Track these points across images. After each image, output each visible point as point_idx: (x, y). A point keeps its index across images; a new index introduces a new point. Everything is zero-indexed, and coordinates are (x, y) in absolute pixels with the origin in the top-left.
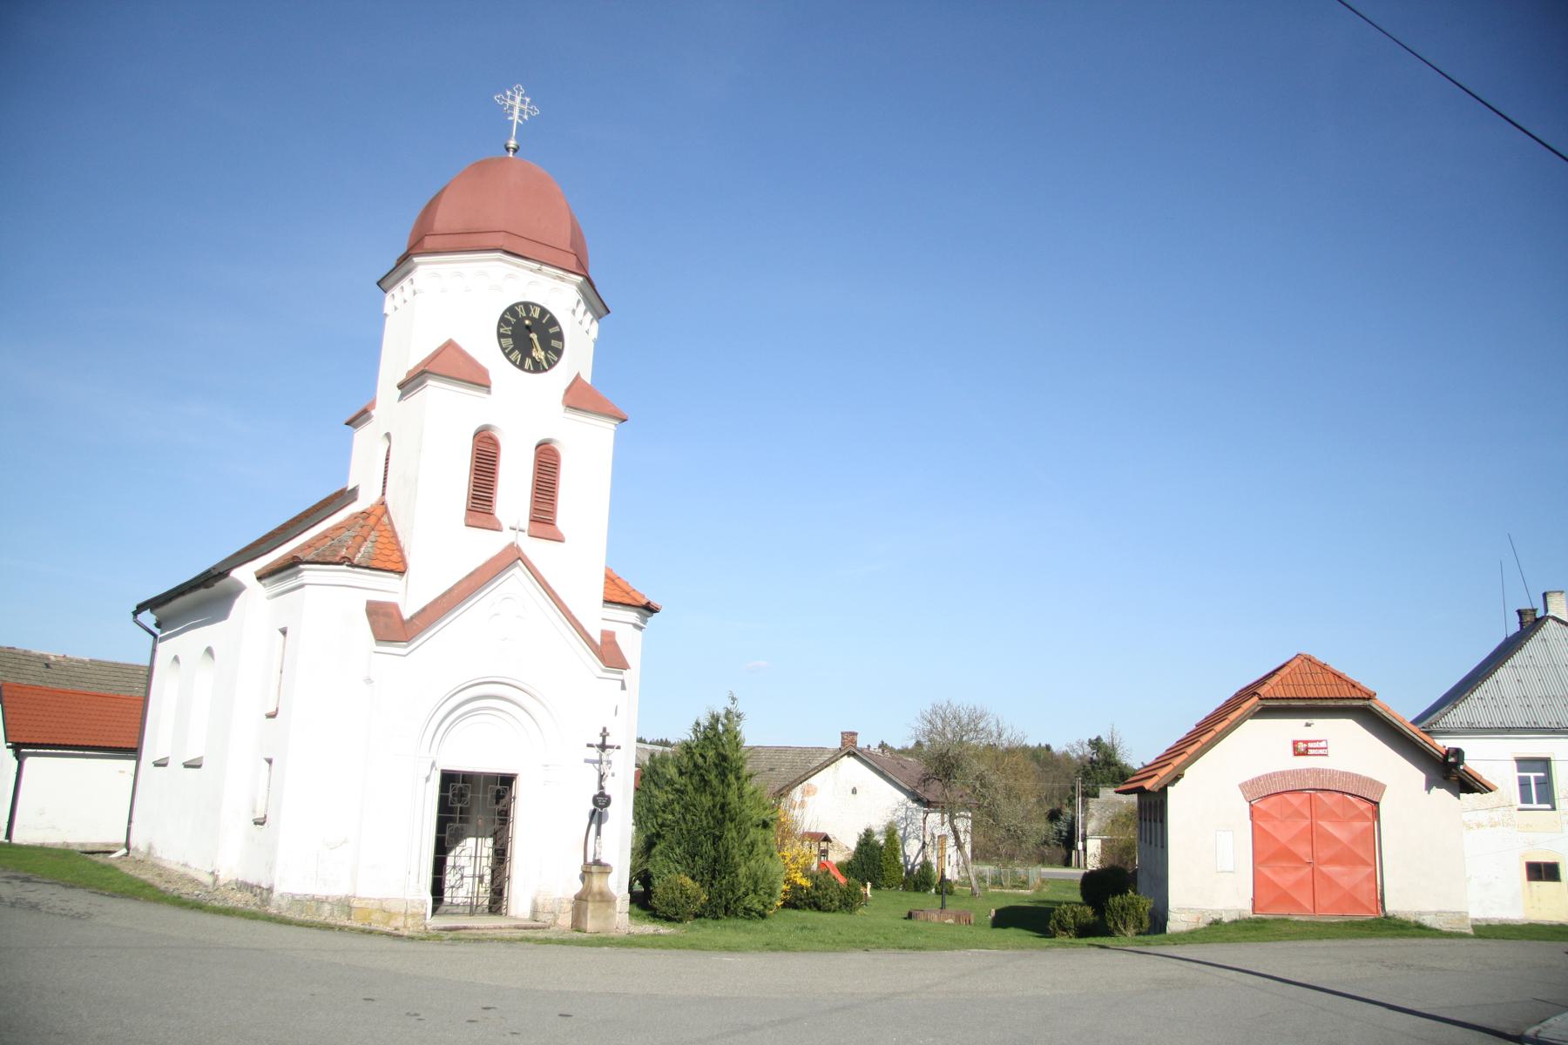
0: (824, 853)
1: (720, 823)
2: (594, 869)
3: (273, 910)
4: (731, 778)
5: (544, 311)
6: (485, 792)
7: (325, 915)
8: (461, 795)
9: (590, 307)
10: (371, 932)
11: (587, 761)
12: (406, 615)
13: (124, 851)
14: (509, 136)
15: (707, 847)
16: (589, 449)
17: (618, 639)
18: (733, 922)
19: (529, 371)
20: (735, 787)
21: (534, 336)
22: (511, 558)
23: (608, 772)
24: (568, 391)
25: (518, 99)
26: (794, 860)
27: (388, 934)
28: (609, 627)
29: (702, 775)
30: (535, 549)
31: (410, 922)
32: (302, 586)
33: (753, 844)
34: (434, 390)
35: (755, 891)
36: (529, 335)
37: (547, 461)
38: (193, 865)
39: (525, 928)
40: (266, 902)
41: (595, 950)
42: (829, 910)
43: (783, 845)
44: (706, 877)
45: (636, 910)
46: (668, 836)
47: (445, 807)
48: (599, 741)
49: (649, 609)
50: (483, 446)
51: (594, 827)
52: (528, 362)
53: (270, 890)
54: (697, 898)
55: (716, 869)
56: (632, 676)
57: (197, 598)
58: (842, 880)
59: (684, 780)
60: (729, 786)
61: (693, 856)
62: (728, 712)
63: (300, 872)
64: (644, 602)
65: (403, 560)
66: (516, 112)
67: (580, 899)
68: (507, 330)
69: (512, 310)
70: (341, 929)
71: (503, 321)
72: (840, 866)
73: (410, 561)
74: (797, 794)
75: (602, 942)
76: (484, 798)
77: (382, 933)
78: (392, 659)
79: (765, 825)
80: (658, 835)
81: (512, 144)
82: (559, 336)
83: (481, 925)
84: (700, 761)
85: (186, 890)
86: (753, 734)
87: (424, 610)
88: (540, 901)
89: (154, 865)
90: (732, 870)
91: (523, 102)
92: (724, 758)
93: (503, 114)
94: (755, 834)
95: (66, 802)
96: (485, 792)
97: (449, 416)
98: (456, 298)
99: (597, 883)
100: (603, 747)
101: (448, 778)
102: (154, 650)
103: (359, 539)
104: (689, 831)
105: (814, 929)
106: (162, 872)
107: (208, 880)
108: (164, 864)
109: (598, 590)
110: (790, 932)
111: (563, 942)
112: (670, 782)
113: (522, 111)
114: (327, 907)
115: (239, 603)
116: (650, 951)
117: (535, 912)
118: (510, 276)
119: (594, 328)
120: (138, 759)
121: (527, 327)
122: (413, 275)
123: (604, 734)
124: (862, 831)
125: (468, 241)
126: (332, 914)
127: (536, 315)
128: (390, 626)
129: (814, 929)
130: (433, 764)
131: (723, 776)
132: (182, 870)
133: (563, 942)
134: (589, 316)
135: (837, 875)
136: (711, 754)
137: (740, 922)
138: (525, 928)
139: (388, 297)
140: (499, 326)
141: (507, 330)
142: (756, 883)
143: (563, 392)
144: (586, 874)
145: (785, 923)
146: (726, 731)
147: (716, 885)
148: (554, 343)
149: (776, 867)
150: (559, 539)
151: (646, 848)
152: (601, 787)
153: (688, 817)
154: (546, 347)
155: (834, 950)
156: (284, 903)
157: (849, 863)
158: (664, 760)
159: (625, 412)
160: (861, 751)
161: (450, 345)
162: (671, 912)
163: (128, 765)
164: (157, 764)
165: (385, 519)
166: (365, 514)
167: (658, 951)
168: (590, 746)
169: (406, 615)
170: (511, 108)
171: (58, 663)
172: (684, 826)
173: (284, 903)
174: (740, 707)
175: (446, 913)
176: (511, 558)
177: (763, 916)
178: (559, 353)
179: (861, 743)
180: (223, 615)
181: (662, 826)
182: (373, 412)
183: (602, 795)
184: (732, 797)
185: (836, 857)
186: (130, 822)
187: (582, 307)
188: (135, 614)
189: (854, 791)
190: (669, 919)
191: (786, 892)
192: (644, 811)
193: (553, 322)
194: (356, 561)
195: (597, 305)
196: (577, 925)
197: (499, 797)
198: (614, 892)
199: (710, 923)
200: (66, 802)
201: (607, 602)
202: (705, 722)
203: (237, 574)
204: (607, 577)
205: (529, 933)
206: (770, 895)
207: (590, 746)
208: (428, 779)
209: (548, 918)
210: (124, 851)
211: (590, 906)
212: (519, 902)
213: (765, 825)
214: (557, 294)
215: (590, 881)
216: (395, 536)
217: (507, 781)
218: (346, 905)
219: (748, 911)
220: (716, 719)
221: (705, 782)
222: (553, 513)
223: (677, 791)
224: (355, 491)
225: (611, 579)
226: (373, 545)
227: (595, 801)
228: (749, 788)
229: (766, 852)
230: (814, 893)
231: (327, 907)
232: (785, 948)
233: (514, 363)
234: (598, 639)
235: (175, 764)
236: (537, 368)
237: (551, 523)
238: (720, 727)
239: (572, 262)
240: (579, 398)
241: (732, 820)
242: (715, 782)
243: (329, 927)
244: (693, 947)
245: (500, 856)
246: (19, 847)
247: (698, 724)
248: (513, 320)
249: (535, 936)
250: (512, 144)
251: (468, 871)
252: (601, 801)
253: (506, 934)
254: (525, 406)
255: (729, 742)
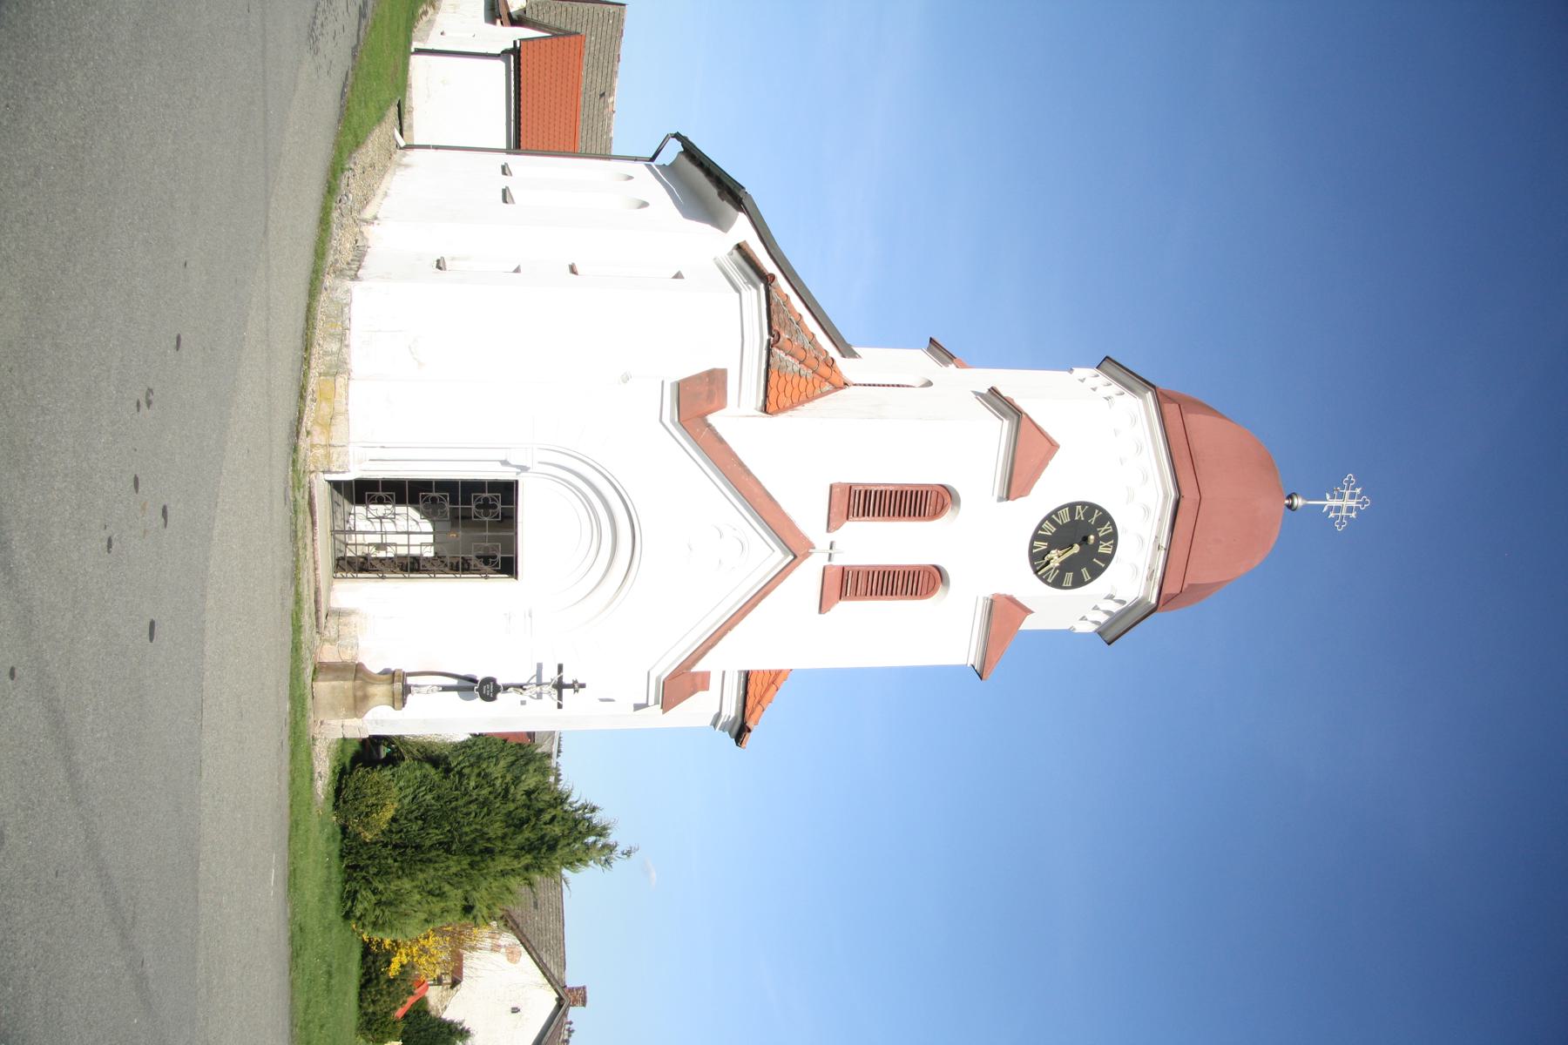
0: (439, 981)
1: (468, 850)
2: (398, 686)
3: (328, 281)
4: (527, 859)
5: (1107, 559)
6: (491, 539)
7: (324, 346)
8: (486, 506)
9: (1115, 618)
10: (302, 397)
11: (540, 667)
12: (711, 419)
13: (402, 144)
14: (1305, 498)
15: (435, 835)
16: (940, 634)
17: (700, 695)
18: (337, 877)
19: (1032, 547)
20: (516, 865)
21: (1076, 548)
22: (795, 548)
23: (526, 696)
24: (1012, 600)
25: (1353, 503)
26: (424, 951)
27: (300, 419)
28: (715, 682)
29: (528, 820)
30: (808, 576)
31: (320, 452)
32: (737, 290)
33: (442, 895)
34: (997, 430)
35: (379, 903)
36: (1076, 543)
37: (918, 582)
38: (385, 202)
39: (316, 602)
40: (340, 273)
41: (285, 691)
42: (361, 999)
43: (443, 933)
44: (395, 837)
45: (351, 750)
46: (447, 784)
47: (470, 488)
48: (567, 680)
49: (740, 732)
50: (932, 499)
51: (454, 682)
52: (1043, 546)
53: (355, 278)
54: (366, 826)
55: (406, 849)
56: (654, 717)
57: (707, 185)
58: (400, 1013)
59: (521, 798)
60: (517, 857)
61: (423, 818)
62: (610, 848)
63: (378, 312)
64: (750, 724)
65: (780, 410)
66: (1335, 503)
67: (357, 671)
68: (1080, 514)
69: (1105, 518)
70: (306, 361)
71: (1091, 508)
72: (423, 1001)
73: (781, 419)
74: (508, 939)
75: (298, 703)
76: (484, 539)
77: (301, 413)
78: (650, 406)
79: (468, 909)
80: (448, 770)
81: (1298, 502)
82: (1079, 582)
83: (319, 544)
84: (547, 817)
85: (352, 184)
86: (581, 888)
87: (721, 441)
88: (353, 619)
89: (385, 169)
90: (406, 871)
91: (1350, 509)
92: (552, 848)
93: (1332, 486)
94: (455, 897)
95: (457, 88)
96: (491, 539)
97: (966, 452)
98: (1109, 448)
99: (380, 691)
100: (560, 686)
101: (507, 491)
102: (636, 159)
103: (802, 354)
104: (455, 809)
105: (329, 989)
106: (378, 171)
107: (368, 213)
108: (387, 177)
109: (760, 662)
110: (323, 957)
111: (296, 648)
112: (517, 781)
113: (1338, 509)
114: (335, 347)
115: (706, 229)
116: (286, 766)
117: (339, 613)
118: (1147, 511)
119: (1089, 628)
120: (508, 151)
121: (1086, 539)
122: (1128, 396)
123: (577, 686)
124: (466, 1025)
125: (1181, 456)
126: (326, 353)
127: (1101, 550)
128: (696, 400)
129: (329, 989)
130: (524, 469)
131: (529, 848)
132: (380, 192)
133: (296, 648)
134: (1103, 618)
135: (411, 1000)
136: (557, 830)
137: (336, 888)
138: (316, 602)
139: (1094, 371)
140: (1083, 504)
141: (1080, 514)
142: (390, 903)
143: (1009, 593)
144: (391, 676)
145: (340, 951)
146: (588, 847)
147: (385, 852)
148: (1069, 576)
149: (413, 928)
150: (823, 608)
151: (434, 757)
152: (506, 688)
153: (473, 807)
154: (1065, 566)
155: (293, 1025)
156: (339, 294)
157: (427, 1013)
158: (544, 771)
159: (991, 677)
160: (565, 1014)
161: (1053, 446)
162: (348, 794)
163: (500, 140)
164: (505, 192)
165: (827, 387)
166: (831, 364)
167: (286, 778)
168: (560, 668)
169: (711, 419)
170: (1341, 496)
171: (606, 105)
172: (461, 802)
173: (339, 294)
174: (618, 863)
175: (335, 503)
176: (795, 548)
177: (347, 916)
178: (1057, 583)
179: (574, 1013)
180: (687, 214)
181: (460, 774)
182: (952, 366)
183: (497, 689)
184: (502, 862)
185: (433, 995)
186: (437, 148)
187: (1115, 608)
188: (677, 136)
189: (515, 1010)
190: (338, 792)
191: (379, 944)
192: (481, 747)
193: (1096, 572)
194: (775, 350)
195: (1116, 630)
196: (321, 669)
197: (486, 559)
198: (369, 715)
199: (335, 848)
200: (457, 88)
201: (747, 675)
202: (597, 819)
203: (742, 218)
204: (778, 673)
205: (308, 606)
206: (374, 924)
207: (560, 668)
208: (505, 463)
209: (331, 632)
210: (402, 144)
211: (348, 684)
212: (350, 593)
213: (468, 909)
214: (1129, 576)
215: (382, 682)
216: (809, 399)
217: (508, 567)
218: (339, 368)
219: (353, 896)
220: (602, 832)
221: (521, 825)
222: (856, 595)
223: (507, 790)
224: (853, 355)
225: (774, 678)
226: (797, 367)
227: (489, 681)
228: (514, 883)
229: (431, 913)
230: (383, 979)
231: (335, 347)
232: (295, 955)
233: (1040, 527)
234: (699, 667)
235: (505, 181)
236: (1037, 560)
237: (842, 595)
238: (591, 839)
239: (1172, 588)
240: (1003, 614)
241: (472, 865)
242: (520, 839)
243: (307, 345)
244: (295, 825)
245: (411, 566)
246: (406, 65)
247: (593, 810)
248: (1093, 521)
249: (302, 617)
250: (1298, 502)
251: (388, 526)
252: (488, 689)
253: (306, 575)
254: (985, 548)
255: (573, 853)
